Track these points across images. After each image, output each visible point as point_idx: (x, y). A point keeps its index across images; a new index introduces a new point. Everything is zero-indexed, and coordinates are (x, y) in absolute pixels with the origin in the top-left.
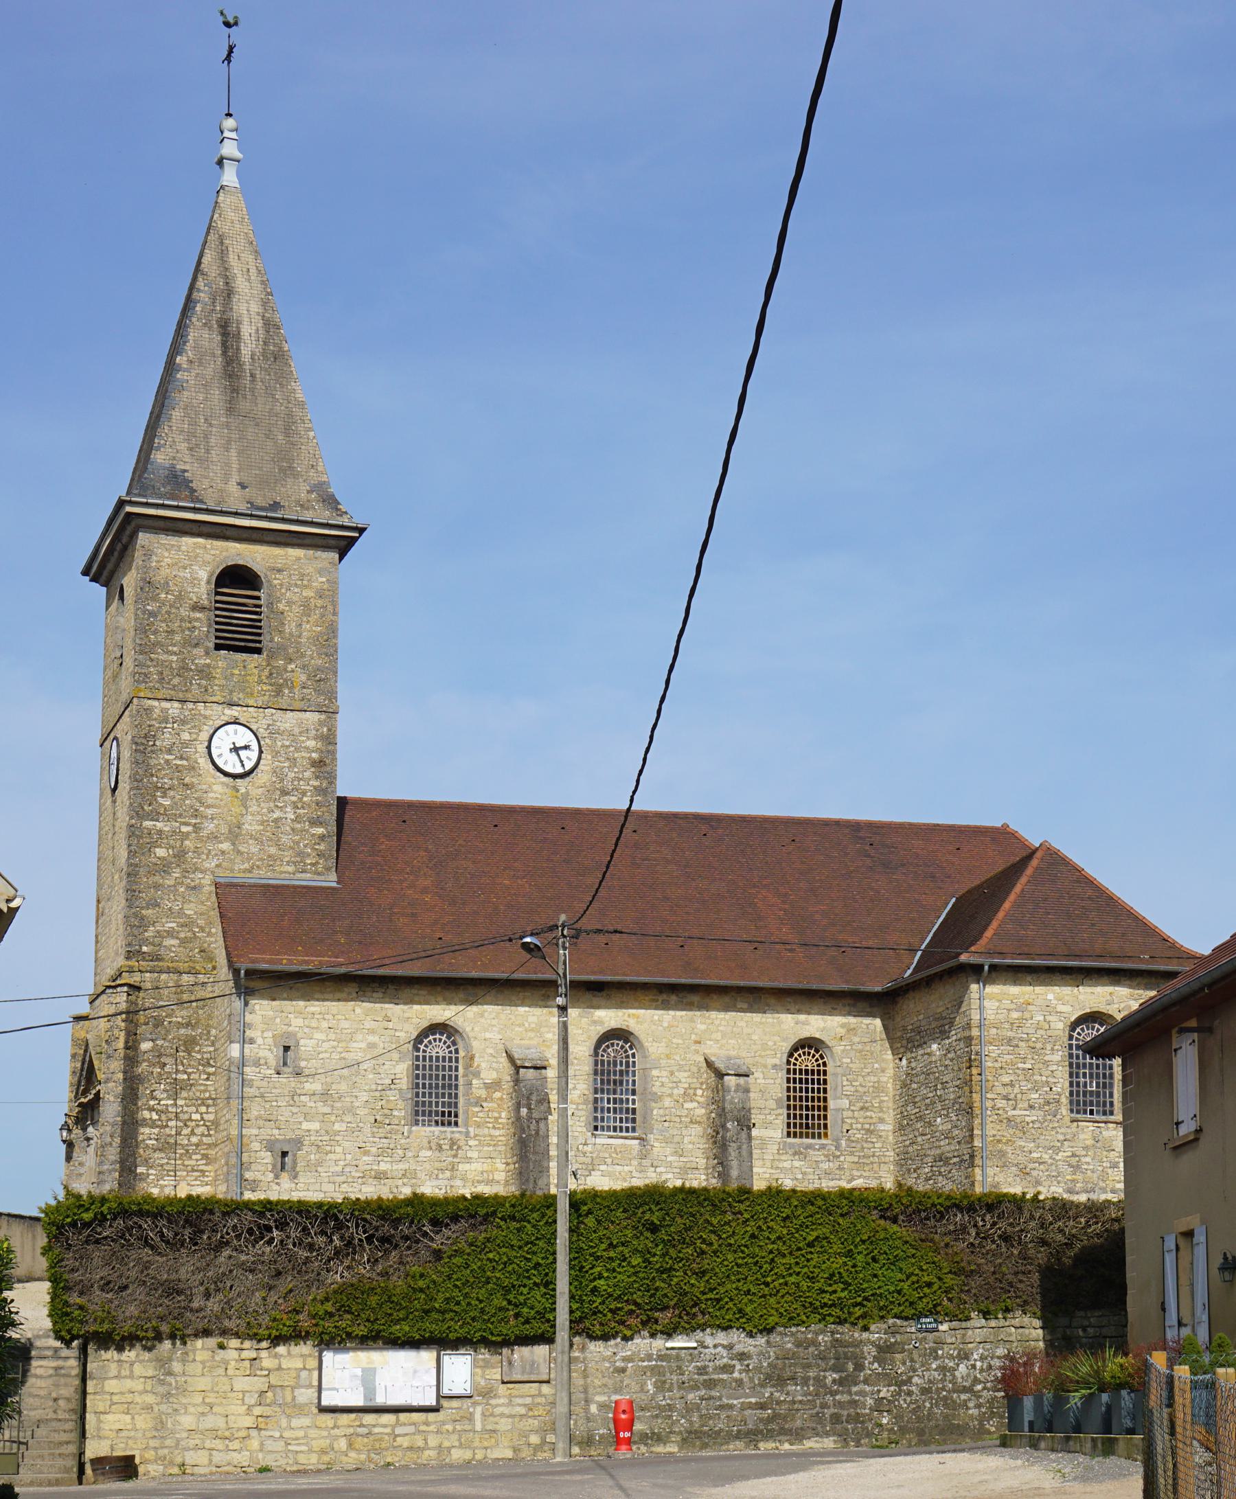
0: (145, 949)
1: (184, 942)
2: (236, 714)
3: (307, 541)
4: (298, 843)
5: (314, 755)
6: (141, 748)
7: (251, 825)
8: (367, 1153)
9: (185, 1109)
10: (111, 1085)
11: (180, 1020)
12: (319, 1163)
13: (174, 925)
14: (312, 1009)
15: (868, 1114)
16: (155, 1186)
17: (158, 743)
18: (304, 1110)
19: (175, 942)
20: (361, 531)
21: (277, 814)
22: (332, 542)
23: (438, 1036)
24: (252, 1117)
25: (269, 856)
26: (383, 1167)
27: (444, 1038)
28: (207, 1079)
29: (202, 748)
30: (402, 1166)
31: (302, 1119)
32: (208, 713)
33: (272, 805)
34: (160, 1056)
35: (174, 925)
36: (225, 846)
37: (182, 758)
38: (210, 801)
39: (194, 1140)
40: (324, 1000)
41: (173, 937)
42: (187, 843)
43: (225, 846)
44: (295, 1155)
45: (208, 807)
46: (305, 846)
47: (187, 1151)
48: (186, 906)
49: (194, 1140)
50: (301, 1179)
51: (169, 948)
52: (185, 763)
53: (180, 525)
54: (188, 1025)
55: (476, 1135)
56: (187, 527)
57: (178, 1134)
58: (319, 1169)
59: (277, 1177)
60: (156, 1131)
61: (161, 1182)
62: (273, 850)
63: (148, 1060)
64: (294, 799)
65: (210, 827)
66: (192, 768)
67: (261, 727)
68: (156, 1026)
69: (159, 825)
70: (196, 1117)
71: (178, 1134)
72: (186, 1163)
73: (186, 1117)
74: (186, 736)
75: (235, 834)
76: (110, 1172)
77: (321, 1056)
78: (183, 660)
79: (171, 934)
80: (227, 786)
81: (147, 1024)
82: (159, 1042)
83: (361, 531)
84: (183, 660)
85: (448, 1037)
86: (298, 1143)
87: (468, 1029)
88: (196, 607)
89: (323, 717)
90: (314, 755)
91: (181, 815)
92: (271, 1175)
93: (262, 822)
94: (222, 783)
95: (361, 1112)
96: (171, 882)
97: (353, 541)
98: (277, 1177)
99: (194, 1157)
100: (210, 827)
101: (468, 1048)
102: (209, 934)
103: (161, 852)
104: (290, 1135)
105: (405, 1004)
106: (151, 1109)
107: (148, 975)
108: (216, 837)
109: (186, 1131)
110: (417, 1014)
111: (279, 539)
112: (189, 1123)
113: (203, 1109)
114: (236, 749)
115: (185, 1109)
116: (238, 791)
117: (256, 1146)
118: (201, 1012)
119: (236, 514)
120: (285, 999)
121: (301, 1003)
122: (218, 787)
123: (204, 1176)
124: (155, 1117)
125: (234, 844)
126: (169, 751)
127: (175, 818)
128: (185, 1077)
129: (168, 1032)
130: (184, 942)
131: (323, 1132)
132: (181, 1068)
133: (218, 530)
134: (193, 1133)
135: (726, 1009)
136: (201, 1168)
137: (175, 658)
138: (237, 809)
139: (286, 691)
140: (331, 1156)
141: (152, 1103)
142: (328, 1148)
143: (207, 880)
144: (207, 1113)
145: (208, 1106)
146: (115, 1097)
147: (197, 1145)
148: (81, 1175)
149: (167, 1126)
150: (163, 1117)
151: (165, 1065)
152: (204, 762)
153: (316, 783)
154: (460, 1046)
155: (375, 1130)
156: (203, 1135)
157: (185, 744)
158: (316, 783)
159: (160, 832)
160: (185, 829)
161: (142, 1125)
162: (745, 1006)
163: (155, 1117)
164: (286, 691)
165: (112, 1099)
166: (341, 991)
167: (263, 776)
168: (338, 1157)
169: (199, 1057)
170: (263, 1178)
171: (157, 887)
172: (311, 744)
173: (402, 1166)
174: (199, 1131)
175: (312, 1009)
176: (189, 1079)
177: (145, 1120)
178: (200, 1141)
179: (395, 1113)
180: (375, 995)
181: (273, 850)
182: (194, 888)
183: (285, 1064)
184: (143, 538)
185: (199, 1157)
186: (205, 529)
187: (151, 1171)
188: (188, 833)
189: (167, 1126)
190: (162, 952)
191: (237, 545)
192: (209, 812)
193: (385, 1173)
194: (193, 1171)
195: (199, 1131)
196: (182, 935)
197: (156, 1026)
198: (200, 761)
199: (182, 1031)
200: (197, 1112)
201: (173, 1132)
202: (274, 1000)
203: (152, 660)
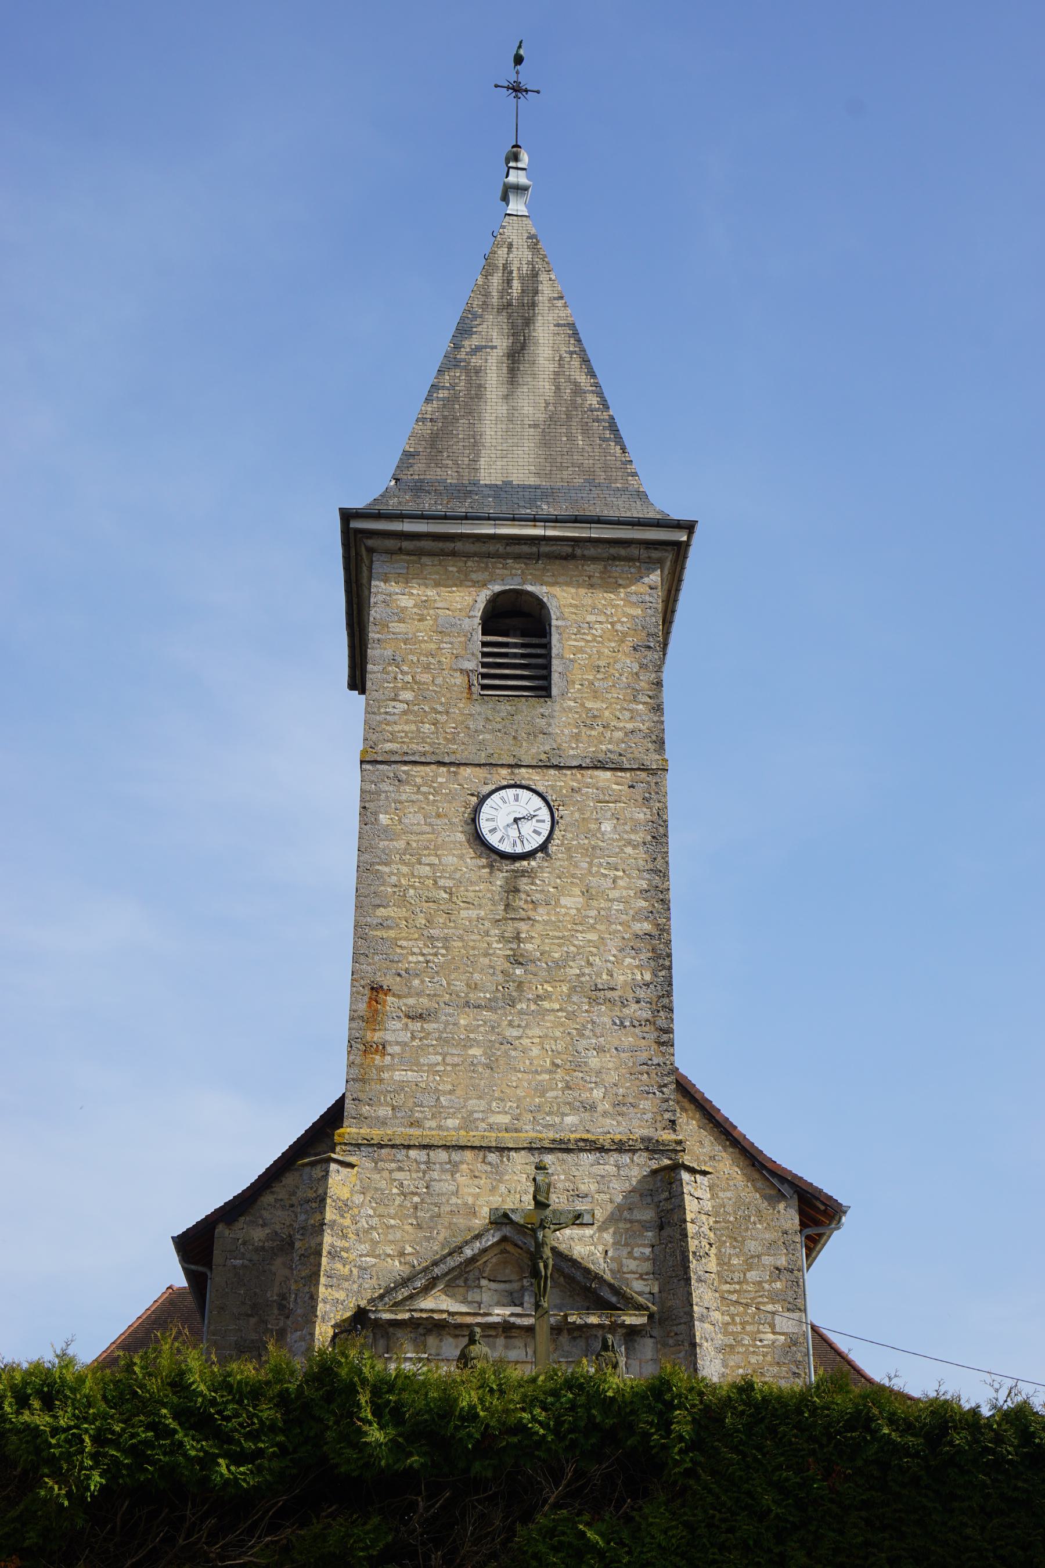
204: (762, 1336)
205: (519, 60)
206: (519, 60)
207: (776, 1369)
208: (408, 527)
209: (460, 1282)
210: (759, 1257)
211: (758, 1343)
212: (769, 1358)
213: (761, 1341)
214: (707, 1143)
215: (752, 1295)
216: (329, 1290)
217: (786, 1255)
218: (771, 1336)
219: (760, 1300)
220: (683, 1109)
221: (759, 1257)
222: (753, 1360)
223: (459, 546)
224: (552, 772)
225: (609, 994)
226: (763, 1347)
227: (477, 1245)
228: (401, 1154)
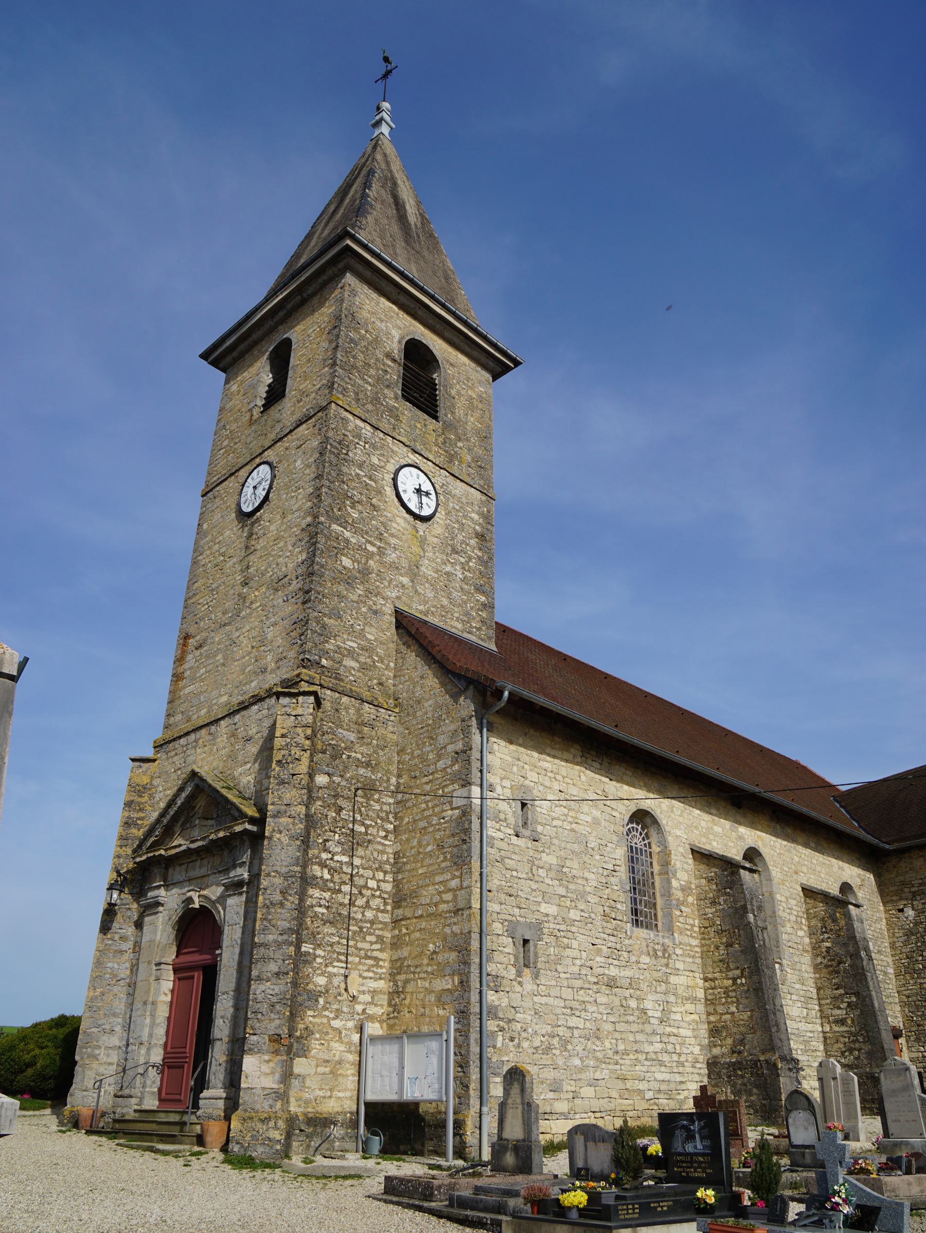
0: (324, 662)
1: (364, 668)
2: (418, 462)
3: (475, 353)
4: (465, 603)
5: (477, 527)
6: (336, 451)
7: (427, 570)
8: (599, 952)
9: (361, 871)
10: (284, 820)
11: (359, 756)
12: (559, 960)
13: (355, 645)
14: (546, 765)
15: (882, 957)
16: (322, 974)
17: (350, 454)
18: (543, 887)
19: (355, 665)
20: (517, 363)
21: (448, 568)
22: (491, 364)
23: (634, 825)
24: (494, 888)
25: (442, 606)
26: (613, 971)
27: (639, 828)
28: (386, 837)
29: (389, 477)
30: (628, 973)
31: (540, 899)
32: (395, 449)
33: (445, 558)
34: (336, 796)
35: (355, 645)
36: (405, 580)
37: (370, 478)
38: (393, 531)
39: (369, 914)
40: (554, 757)
41: (353, 659)
42: (371, 562)
43: (405, 580)
44: (535, 946)
45: (392, 535)
46: (472, 608)
47: (361, 928)
48: (367, 629)
49: (369, 914)
50: (543, 980)
51: (349, 669)
52: (373, 484)
53: (383, 283)
54: (368, 765)
55: (680, 943)
56: (389, 289)
57: (351, 903)
58: (559, 968)
59: (519, 974)
60: (327, 895)
61: (330, 969)
62: (445, 602)
63: (322, 799)
64: (462, 560)
65: (392, 556)
66: (379, 492)
67: (438, 481)
68: (334, 757)
69: (347, 534)
70: (372, 884)
71: (351, 903)
72: (360, 945)
73: (361, 882)
74: (375, 460)
75: (414, 572)
76: (279, 945)
77: (555, 823)
78: (377, 393)
79: (351, 653)
80: (409, 523)
81: (324, 752)
82: (337, 779)
83: (517, 363)
84: (377, 393)
85: (643, 829)
86: (538, 927)
87: (664, 822)
88: (388, 355)
89: (484, 498)
90: (477, 527)
91: (367, 533)
92: (513, 971)
93: (437, 571)
94: (404, 518)
95: (593, 899)
96: (355, 598)
97: (507, 369)
98: (519, 974)
99: (368, 938)
100: (392, 556)
101: (664, 844)
102: (388, 667)
103: (347, 562)
104: (532, 919)
105: (618, 781)
106: (323, 865)
107: (328, 692)
108: (397, 568)
109: (360, 902)
110: (636, 795)
111: (456, 340)
112: (364, 891)
113: (380, 875)
114: (418, 491)
115: (361, 871)
116: (417, 532)
117: (497, 927)
118: (381, 753)
119: (432, 297)
120: (520, 745)
121: (535, 754)
122: (401, 521)
123: (377, 966)
124: (327, 876)
125: (412, 581)
126: (360, 466)
127: (363, 533)
128: (363, 829)
129: (346, 768)
130: (364, 668)
131: (559, 919)
132: (358, 817)
133: (412, 304)
134: (367, 906)
135: (806, 845)
136: (376, 954)
137: (369, 388)
138: (416, 549)
139: (457, 463)
140: (568, 952)
141: (324, 856)
142: (565, 941)
143: (389, 609)
144: (384, 881)
145: (385, 873)
146: (292, 838)
147: (372, 922)
148: (121, 952)
149: (340, 891)
150: (336, 878)
151: (341, 809)
152: (389, 491)
153: (480, 554)
154: (654, 839)
155: (605, 924)
156: (378, 910)
157: (374, 467)
158: (480, 554)
159: (347, 541)
160: (370, 548)
161: (315, 886)
162: (813, 845)
163: (327, 876)
164: (457, 463)
165: (285, 840)
166: (568, 750)
167: (438, 527)
168: (575, 953)
169: (377, 807)
170: (504, 973)
171: (340, 596)
172: (475, 517)
173: (628, 973)
174: (375, 903)
175: (546, 765)
176: (366, 834)
177: (315, 877)
178: (376, 917)
179: (619, 906)
180: (594, 764)
181: (445, 602)
182: (376, 612)
183: (525, 824)
184: (349, 278)
185: (372, 938)
186: (403, 299)
187: (319, 952)
188: (373, 553)
189: (340, 891)
190: (342, 671)
191: (422, 328)
192: (393, 541)
193: (614, 979)
194: (367, 957)
195: (375, 903)
196: (362, 659)
197: (334, 757)
198: (386, 488)
199: (362, 771)
200: (373, 878)
201: (347, 901)
202: (511, 743)
203: (350, 379)
204: (444, 814)
205: (386, 60)
206: (386, 60)
207: (451, 840)
208: (228, 343)
209: (188, 825)
210: (445, 747)
211: (442, 821)
212: (448, 832)
213: (443, 818)
214: (419, 666)
215: (440, 780)
216: (124, 848)
217: (463, 739)
218: (450, 812)
219: (445, 783)
220: (409, 647)
221: (445, 747)
222: (438, 837)
223: (255, 336)
224: (279, 444)
225: (286, 579)
226: (444, 823)
227: (184, 795)
228: (176, 744)
